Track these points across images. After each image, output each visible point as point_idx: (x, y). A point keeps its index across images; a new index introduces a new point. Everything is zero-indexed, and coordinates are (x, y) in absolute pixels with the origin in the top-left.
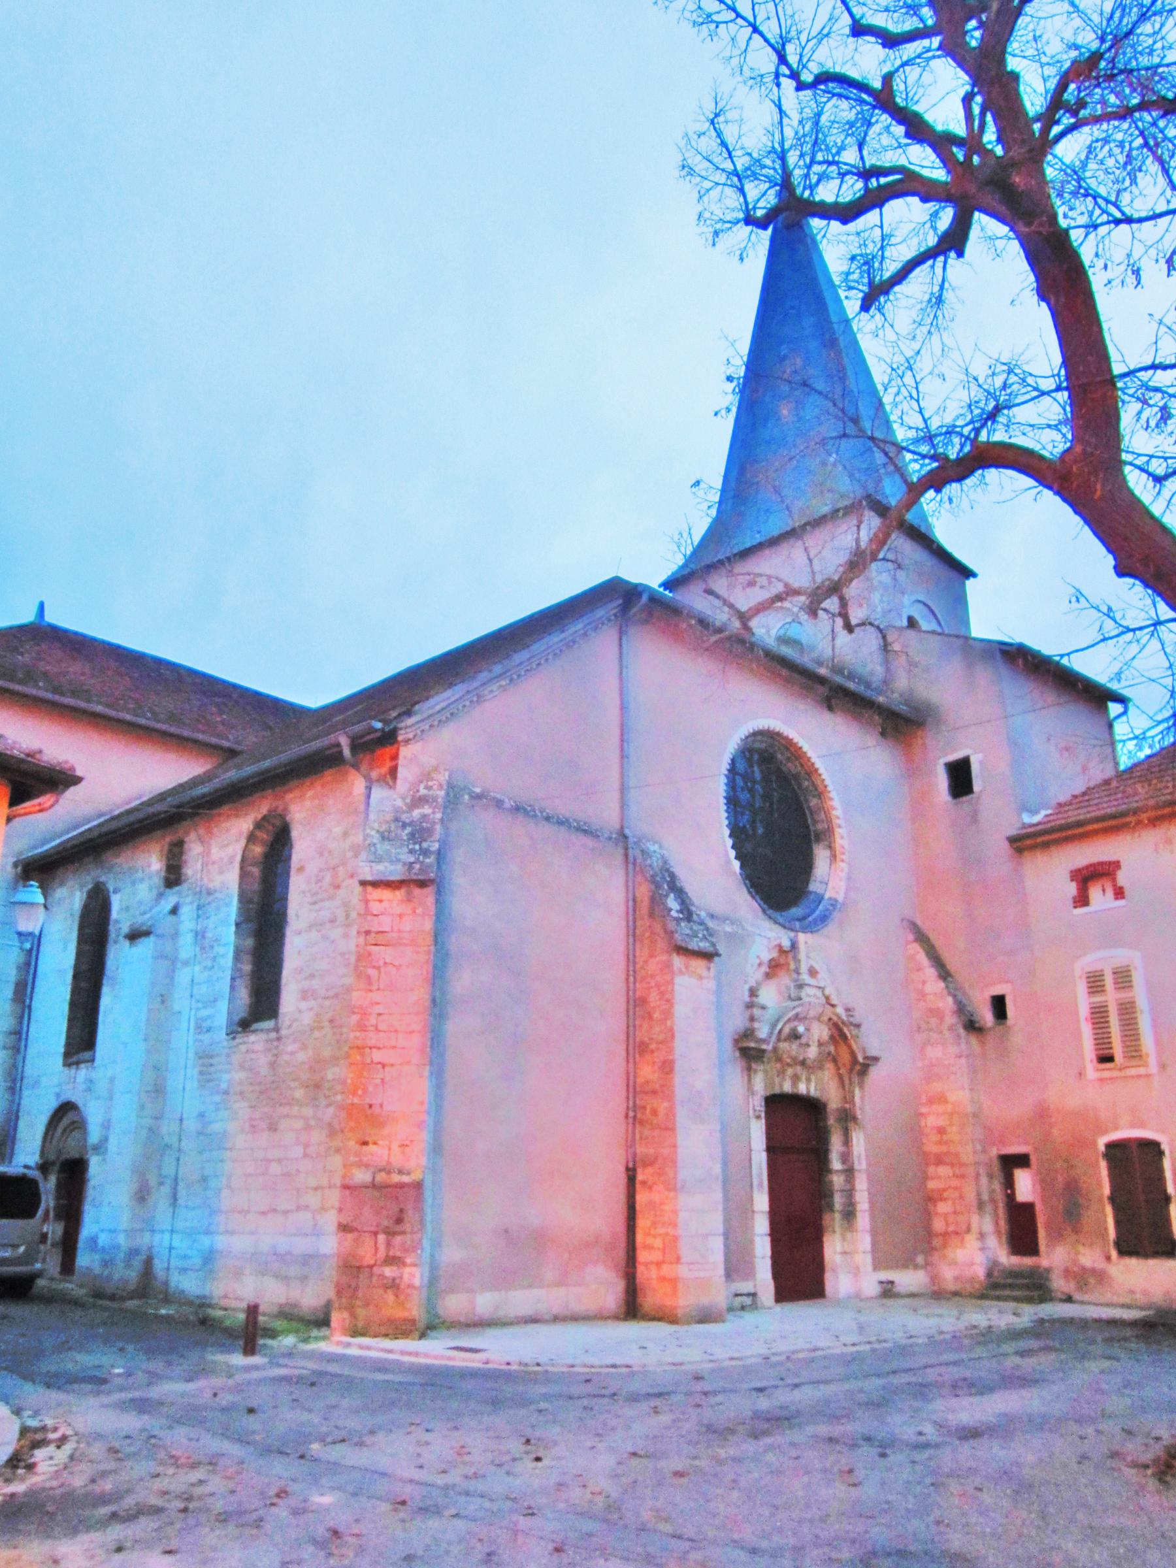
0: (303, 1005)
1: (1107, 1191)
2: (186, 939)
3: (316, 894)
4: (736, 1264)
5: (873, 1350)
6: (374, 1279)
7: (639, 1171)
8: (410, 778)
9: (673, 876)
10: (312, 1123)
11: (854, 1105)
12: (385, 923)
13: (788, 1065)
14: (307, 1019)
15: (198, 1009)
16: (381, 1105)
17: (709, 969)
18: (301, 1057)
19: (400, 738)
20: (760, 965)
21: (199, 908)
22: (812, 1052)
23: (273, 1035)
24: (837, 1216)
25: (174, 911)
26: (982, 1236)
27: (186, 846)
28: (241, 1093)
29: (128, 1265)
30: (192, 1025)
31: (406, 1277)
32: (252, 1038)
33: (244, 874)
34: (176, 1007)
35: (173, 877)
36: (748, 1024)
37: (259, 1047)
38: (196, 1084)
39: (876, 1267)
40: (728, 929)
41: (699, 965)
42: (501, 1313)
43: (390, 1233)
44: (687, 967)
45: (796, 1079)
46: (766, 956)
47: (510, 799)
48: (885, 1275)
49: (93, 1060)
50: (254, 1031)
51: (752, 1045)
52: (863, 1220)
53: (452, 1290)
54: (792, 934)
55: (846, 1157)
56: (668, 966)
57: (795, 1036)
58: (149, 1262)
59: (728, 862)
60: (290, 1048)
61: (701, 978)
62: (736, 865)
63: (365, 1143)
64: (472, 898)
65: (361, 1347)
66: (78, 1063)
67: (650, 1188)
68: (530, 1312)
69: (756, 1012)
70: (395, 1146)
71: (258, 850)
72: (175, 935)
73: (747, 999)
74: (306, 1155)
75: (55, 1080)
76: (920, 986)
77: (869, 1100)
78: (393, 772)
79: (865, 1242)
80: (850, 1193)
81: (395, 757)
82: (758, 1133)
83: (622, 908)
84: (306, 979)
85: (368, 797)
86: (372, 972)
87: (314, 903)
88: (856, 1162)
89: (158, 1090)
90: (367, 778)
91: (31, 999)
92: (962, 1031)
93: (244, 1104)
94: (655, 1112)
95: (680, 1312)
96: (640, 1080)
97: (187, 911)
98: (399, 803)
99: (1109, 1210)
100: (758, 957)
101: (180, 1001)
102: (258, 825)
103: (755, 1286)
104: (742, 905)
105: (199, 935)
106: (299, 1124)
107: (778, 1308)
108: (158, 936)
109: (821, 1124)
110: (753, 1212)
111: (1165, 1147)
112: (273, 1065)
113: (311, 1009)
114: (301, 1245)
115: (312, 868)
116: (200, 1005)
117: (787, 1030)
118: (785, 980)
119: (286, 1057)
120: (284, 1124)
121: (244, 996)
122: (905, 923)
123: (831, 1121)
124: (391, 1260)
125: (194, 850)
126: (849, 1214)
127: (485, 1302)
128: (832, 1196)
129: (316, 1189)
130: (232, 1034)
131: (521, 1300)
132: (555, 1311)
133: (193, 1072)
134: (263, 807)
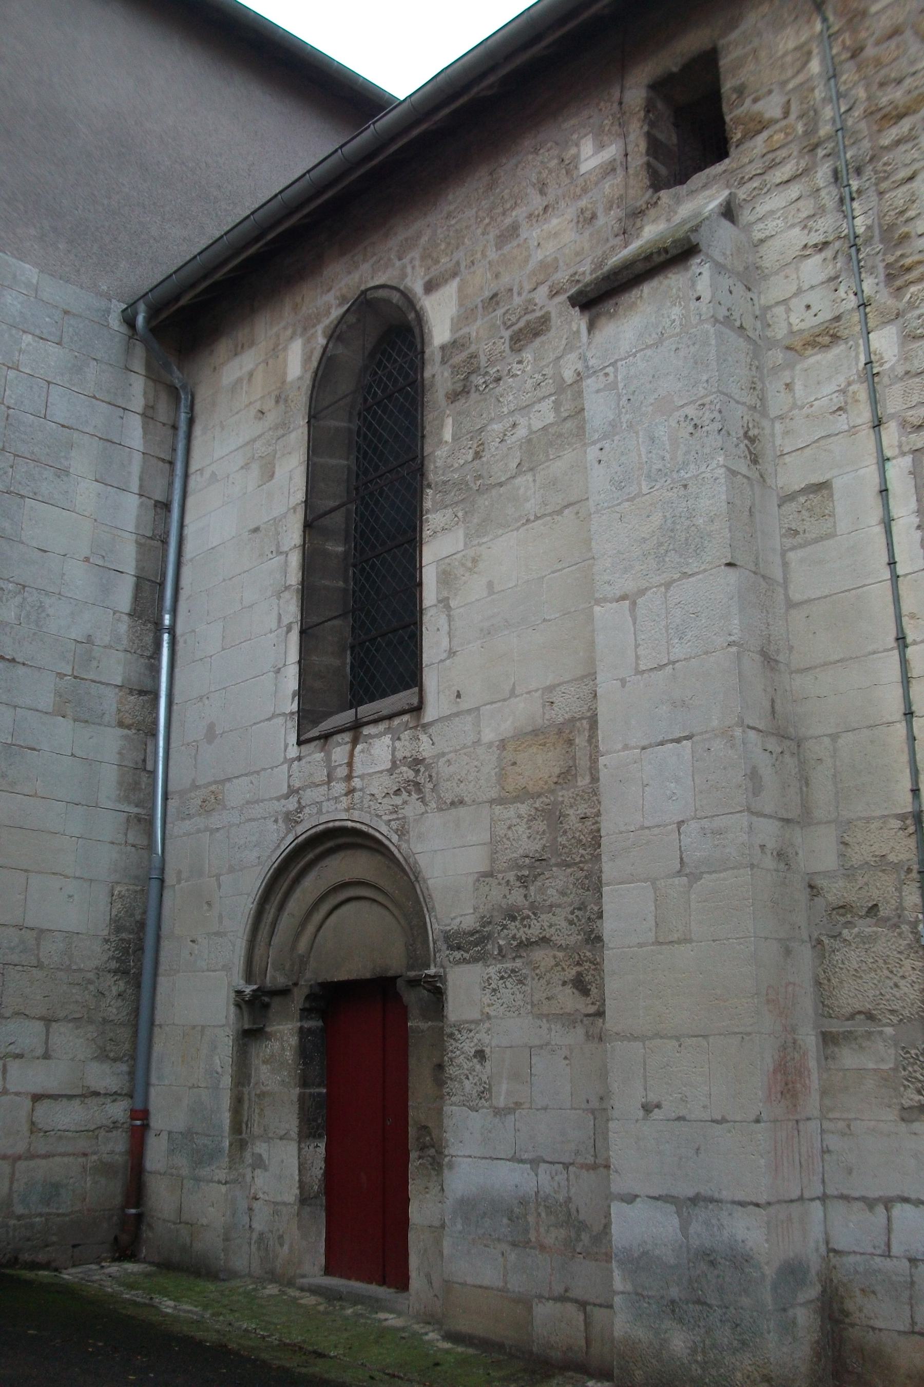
5: (533, 1342)
29: (788, 1328)
49: (417, 709)
66: (326, 737)
75: (279, 781)
91: (174, 612)
109: (314, 1023)
134: (327, 298)
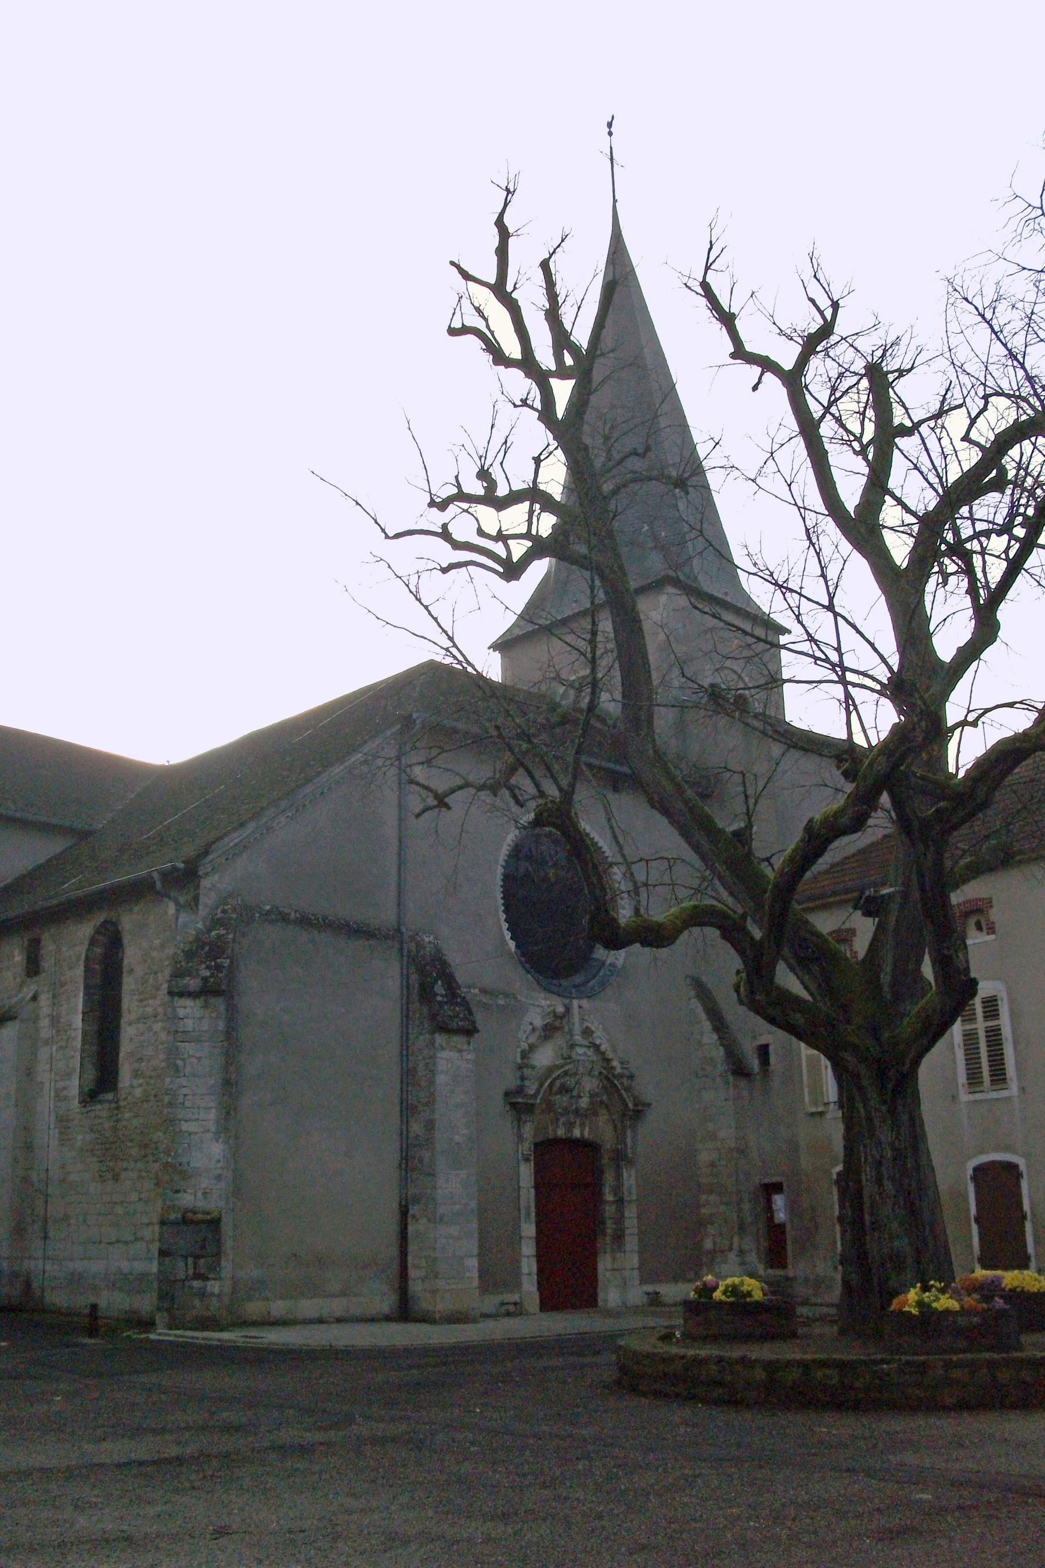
0: (135, 1082)
1: (973, 1211)
2: (45, 1022)
3: (142, 993)
4: (494, 1276)
6: (186, 1290)
7: (410, 1207)
8: (210, 903)
9: (445, 964)
10: (144, 1174)
11: (626, 1145)
12: (189, 1025)
13: (562, 1115)
14: (138, 1092)
15: (56, 1081)
16: (188, 1163)
17: (469, 1043)
18: (135, 1122)
19: (200, 873)
20: (534, 1030)
21: (54, 997)
22: (584, 1102)
23: (113, 1105)
24: (608, 1239)
25: (35, 998)
26: (741, 1252)
27: (43, 943)
28: (92, 1150)
30: (52, 1094)
31: (209, 1288)
32: (99, 1107)
33: (88, 969)
34: (39, 1079)
35: (33, 967)
36: (519, 1082)
37: (105, 1114)
38: (57, 1142)
39: (643, 1281)
40: (501, 1002)
41: (459, 1040)
42: (290, 1316)
43: (197, 1257)
44: (448, 1043)
45: (570, 1126)
46: (538, 1022)
47: (296, 911)
48: (649, 1288)
50: (100, 1102)
51: (520, 1100)
52: (631, 1242)
53: (250, 1299)
54: (567, 1001)
55: (617, 1189)
56: (432, 1043)
57: (565, 1089)
58: (28, 1284)
59: (504, 942)
60: (127, 1116)
61: (460, 1051)
62: (512, 945)
63: (177, 1191)
64: (259, 996)
65: (175, 1335)
67: (417, 1220)
68: (317, 1315)
69: (527, 1072)
70: (199, 1194)
71: (98, 951)
72: (36, 1019)
73: (519, 1060)
74: (140, 1199)
76: (699, 1037)
77: (647, 1138)
78: (196, 899)
79: (632, 1260)
80: (619, 1220)
81: (198, 887)
82: (526, 1173)
83: (398, 993)
84: (137, 1061)
85: (177, 918)
86: (180, 1063)
87: (141, 1001)
88: (626, 1193)
89: (28, 1147)
90: (177, 903)
92: (731, 1078)
93: (95, 1159)
94: (421, 1161)
95: (437, 1316)
96: (411, 1135)
97: (44, 1000)
98: (200, 925)
99: (975, 1228)
100: (531, 1024)
101: (44, 1075)
102: (98, 932)
103: (521, 1298)
104: (519, 980)
105: (55, 1020)
106: (134, 1175)
107: (544, 1315)
108: (22, 1021)
110: (521, 1238)
111: (1023, 1168)
112: (115, 1129)
113: (141, 1085)
114: (139, 1267)
115: (139, 971)
116: (58, 1078)
117: (558, 1083)
118: (559, 1041)
119: (124, 1123)
120: (123, 1175)
121: (91, 1074)
122: (688, 981)
123: (605, 1161)
124: (198, 1276)
125: (48, 946)
126: (619, 1237)
127: (279, 1308)
128: (604, 1223)
129: (148, 1225)
130: (83, 1102)
131: (308, 1307)
132: (337, 1314)
133: (55, 1133)
134: (100, 917)
